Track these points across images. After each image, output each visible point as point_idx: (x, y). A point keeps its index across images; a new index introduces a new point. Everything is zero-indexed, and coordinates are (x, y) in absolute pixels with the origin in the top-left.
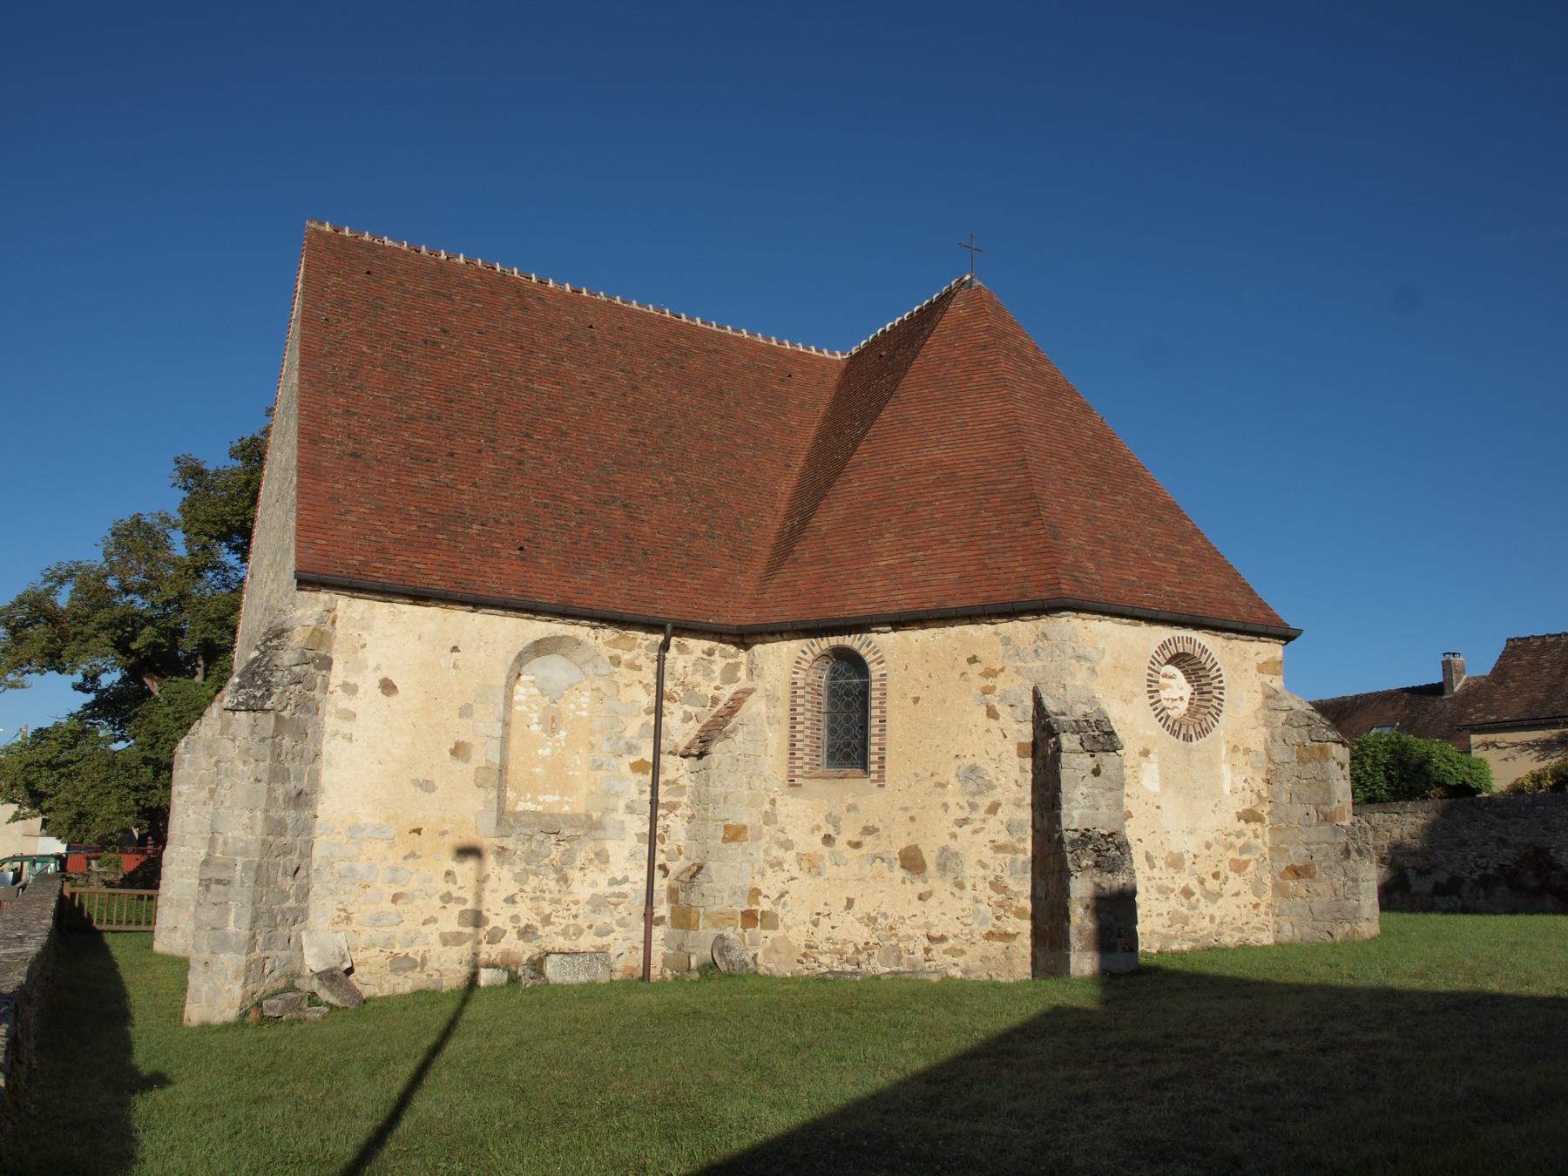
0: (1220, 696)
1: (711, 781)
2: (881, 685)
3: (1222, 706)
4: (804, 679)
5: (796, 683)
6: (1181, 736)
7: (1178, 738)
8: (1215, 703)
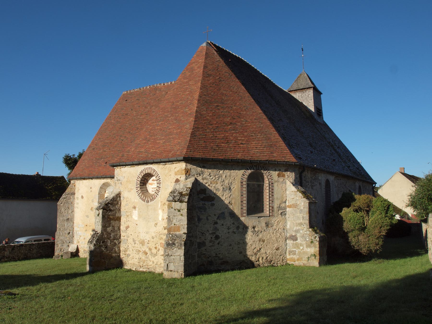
3: (160, 189)
7: (144, 202)
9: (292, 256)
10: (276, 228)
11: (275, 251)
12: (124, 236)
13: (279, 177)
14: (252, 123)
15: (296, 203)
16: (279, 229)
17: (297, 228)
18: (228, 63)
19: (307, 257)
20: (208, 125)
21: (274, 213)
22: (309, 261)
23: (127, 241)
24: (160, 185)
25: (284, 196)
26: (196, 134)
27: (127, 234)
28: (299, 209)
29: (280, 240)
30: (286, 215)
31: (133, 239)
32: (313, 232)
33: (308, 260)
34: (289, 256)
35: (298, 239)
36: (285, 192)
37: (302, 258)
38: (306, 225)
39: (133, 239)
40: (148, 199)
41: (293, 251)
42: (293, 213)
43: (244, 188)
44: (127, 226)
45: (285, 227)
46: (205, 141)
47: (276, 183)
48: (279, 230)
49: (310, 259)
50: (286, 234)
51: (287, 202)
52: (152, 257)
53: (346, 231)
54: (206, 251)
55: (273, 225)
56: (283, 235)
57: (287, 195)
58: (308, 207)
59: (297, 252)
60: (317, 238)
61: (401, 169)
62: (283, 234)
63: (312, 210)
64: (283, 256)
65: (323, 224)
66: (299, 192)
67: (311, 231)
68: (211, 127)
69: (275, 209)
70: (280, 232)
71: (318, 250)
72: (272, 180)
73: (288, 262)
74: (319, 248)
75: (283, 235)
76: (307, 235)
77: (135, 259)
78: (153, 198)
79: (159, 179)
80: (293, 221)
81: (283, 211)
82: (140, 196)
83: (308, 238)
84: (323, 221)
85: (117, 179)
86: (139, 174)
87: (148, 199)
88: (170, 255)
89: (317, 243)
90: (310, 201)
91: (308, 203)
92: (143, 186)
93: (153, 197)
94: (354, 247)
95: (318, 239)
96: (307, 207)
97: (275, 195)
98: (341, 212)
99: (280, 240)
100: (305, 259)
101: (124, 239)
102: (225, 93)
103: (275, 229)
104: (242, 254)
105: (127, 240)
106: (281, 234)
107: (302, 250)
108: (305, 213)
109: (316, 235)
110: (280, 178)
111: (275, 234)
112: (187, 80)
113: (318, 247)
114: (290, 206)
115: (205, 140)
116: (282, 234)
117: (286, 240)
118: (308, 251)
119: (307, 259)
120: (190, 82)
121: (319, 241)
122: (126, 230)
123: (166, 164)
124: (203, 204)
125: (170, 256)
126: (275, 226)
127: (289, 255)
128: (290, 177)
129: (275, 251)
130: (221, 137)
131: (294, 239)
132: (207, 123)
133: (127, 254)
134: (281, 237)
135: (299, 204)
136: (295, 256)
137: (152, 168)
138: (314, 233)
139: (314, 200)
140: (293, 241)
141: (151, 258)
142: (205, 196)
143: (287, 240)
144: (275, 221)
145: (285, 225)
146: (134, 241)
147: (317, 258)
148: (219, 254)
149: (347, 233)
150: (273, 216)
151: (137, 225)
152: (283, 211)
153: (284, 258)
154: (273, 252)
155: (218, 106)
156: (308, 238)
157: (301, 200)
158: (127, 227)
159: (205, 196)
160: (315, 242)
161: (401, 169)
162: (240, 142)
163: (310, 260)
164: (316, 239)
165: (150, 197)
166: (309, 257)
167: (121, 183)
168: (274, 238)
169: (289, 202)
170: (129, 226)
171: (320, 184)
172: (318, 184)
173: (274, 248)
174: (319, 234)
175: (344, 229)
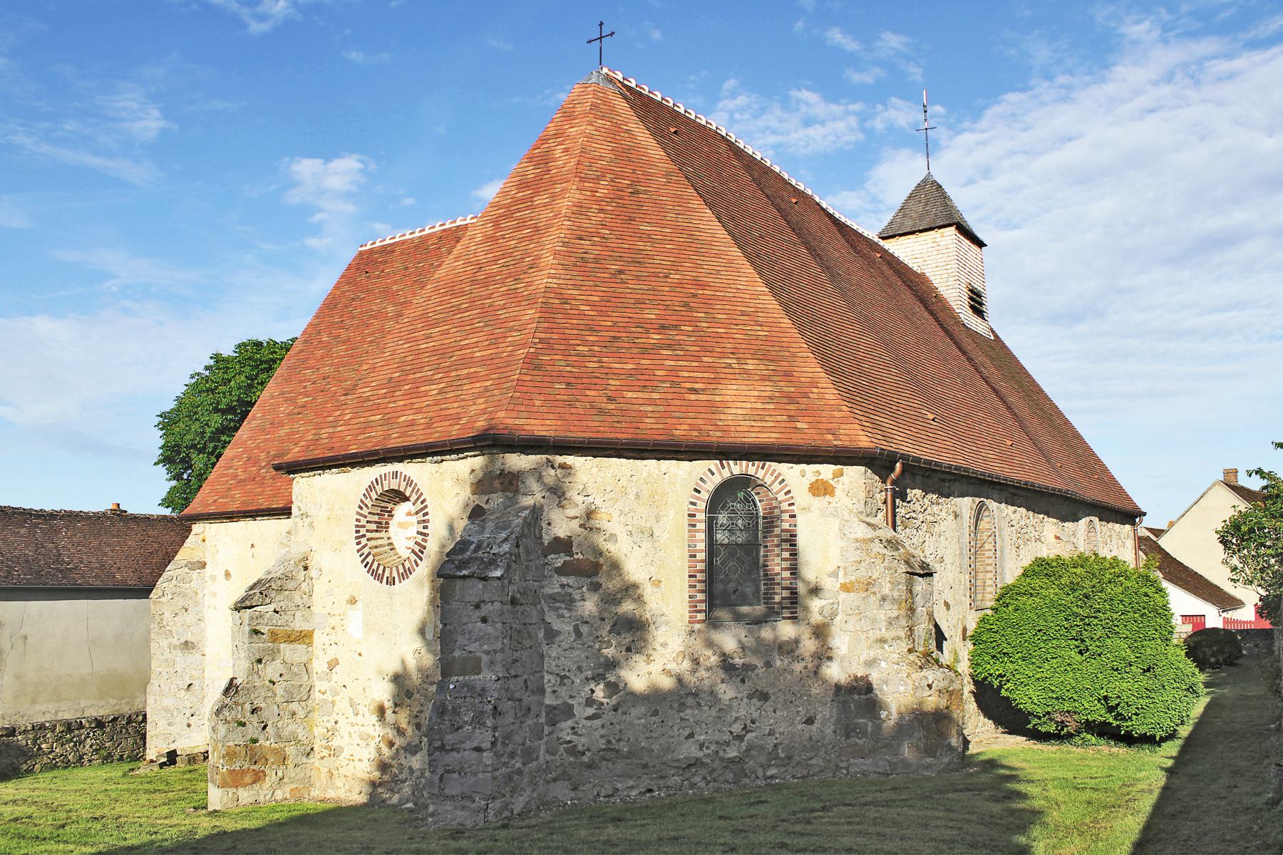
0: (425, 531)
1: (923, 309)
2: (780, 483)
3: (426, 541)
4: (780, 502)
5: (699, 492)
6: (385, 579)
7: (381, 582)
8: (365, 511)
12: (323, 690)
14: (732, 326)
18: (659, 134)
20: (583, 333)
23: (331, 706)
24: (426, 527)
26: (543, 362)
27: (333, 683)
31: (351, 699)
39: (351, 699)
40: (391, 573)
43: (699, 531)
44: (332, 660)
46: (568, 384)
52: (408, 755)
54: (575, 733)
61: (1227, 472)
68: (591, 338)
72: (793, 504)
77: (357, 761)
78: (405, 571)
79: (422, 509)
82: (368, 563)
85: (301, 512)
86: (364, 495)
87: (391, 573)
88: (448, 748)
92: (377, 531)
93: (407, 565)
101: (324, 700)
102: (647, 232)
104: (692, 740)
105: (333, 703)
112: (529, 192)
115: (572, 380)
120: (536, 199)
122: (328, 671)
123: (442, 461)
124: (562, 586)
125: (448, 751)
130: (624, 372)
132: (583, 327)
133: (333, 749)
137: (401, 473)
141: (405, 758)
142: (568, 558)
146: (352, 704)
148: (619, 740)
151: (360, 655)
155: (621, 272)
158: (333, 665)
159: (568, 558)
161: (1227, 472)
162: (688, 385)
165: (397, 567)
167: (311, 525)
170: (337, 659)
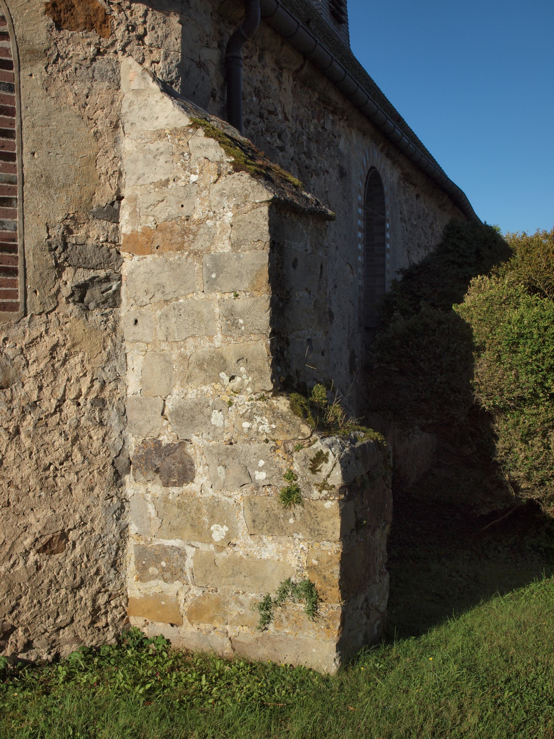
9: (161, 582)
10: (34, 397)
11: (32, 557)
13: (59, 25)
15: (186, 211)
16: (62, 400)
17: (192, 394)
19: (253, 603)
21: (20, 288)
22: (271, 627)
25: (104, 164)
28: (206, 258)
29: (72, 477)
30: (116, 304)
32: (298, 420)
33: (267, 619)
34: (139, 584)
35: (199, 469)
36: (107, 140)
37: (220, 605)
38: (249, 372)
41: (165, 549)
42: (161, 287)
45: (110, 387)
47: (40, 66)
48: (59, 408)
49: (277, 612)
50: (115, 435)
51: (125, 215)
53: (486, 404)
55: (12, 372)
56: (96, 444)
57: (127, 166)
58: (267, 238)
59: (189, 563)
60: (326, 467)
62: (97, 434)
63: (295, 265)
64: (97, 585)
65: (352, 368)
66: (201, 132)
67: (282, 416)
69: (30, 259)
70: (72, 421)
71: (337, 558)
73: (136, 621)
74: (344, 537)
75: (96, 444)
76: (255, 447)
80: (165, 346)
81: (92, 273)
83: (262, 463)
84: (353, 356)
89: (328, 504)
90: (281, 193)
91: (265, 209)
94: (517, 489)
95: (338, 473)
96: (257, 235)
97: (26, 158)
98: (460, 300)
99: (72, 477)
100: (243, 611)
103: (34, 405)
106: (76, 439)
107: (220, 548)
108: (246, 285)
109: (319, 446)
110: (67, 33)
111: (26, 442)
113: (338, 534)
114: (144, 239)
116: (85, 441)
117: (117, 475)
118: (266, 555)
119: (258, 616)
121: (342, 489)
126: (30, 386)
127: (142, 577)
128: (147, 40)
129: (32, 557)
131: (170, 474)
134: (78, 457)
135: (201, 222)
136: (177, 585)
138: (306, 429)
139: (307, 199)
140: (166, 484)
143: (128, 478)
144: (33, 342)
145: (108, 375)
147: (323, 609)
149: (489, 417)
150: (13, 307)
152: (92, 273)
153: (102, 599)
154: (20, 567)
156: (262, 463)
157: (217, 186)
160: (316, 494)
163: (280, 624)
164: (324, 474)
166: (268, 598)
168: (26, 471)
169: (134, 214)
171: (343, 174)
172: (334, 174)
173: (28, 542)
174: (345, 438)
175: (478, 396)
